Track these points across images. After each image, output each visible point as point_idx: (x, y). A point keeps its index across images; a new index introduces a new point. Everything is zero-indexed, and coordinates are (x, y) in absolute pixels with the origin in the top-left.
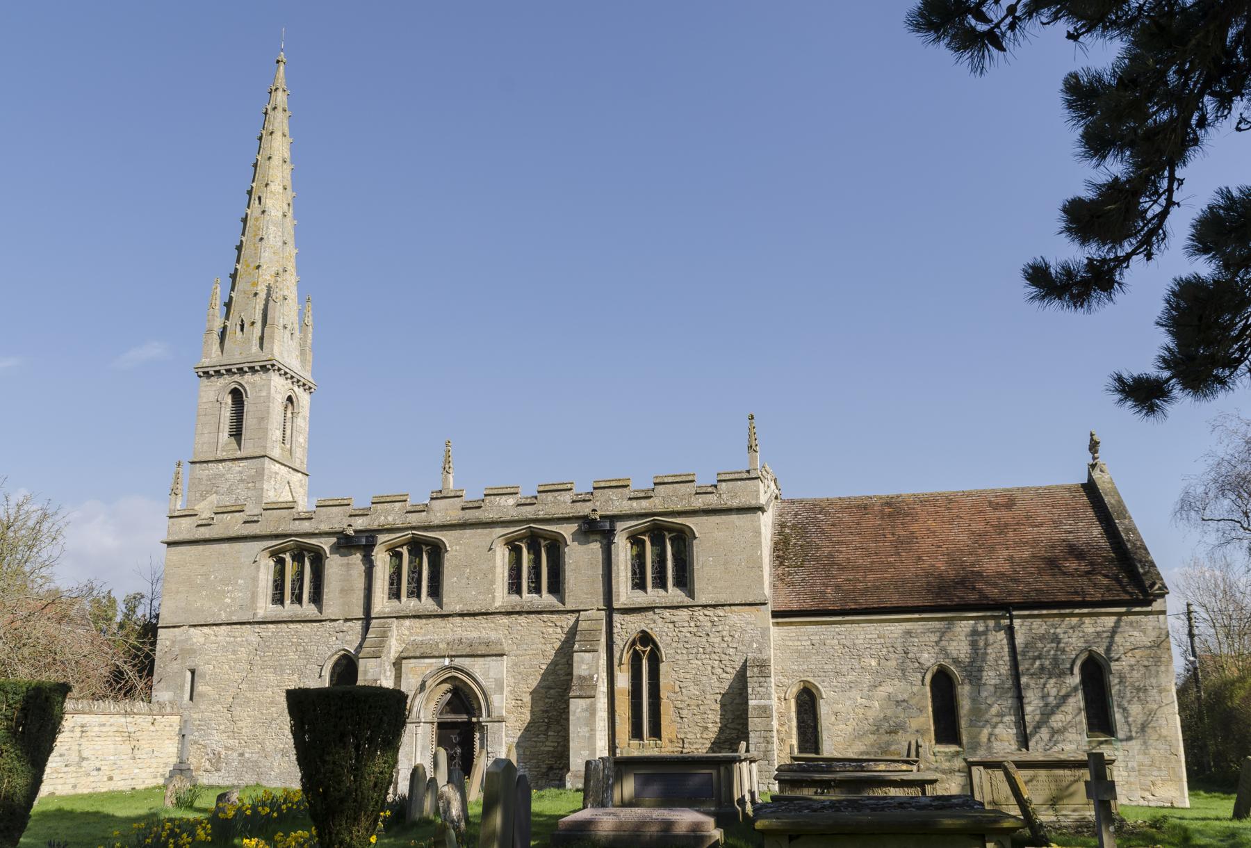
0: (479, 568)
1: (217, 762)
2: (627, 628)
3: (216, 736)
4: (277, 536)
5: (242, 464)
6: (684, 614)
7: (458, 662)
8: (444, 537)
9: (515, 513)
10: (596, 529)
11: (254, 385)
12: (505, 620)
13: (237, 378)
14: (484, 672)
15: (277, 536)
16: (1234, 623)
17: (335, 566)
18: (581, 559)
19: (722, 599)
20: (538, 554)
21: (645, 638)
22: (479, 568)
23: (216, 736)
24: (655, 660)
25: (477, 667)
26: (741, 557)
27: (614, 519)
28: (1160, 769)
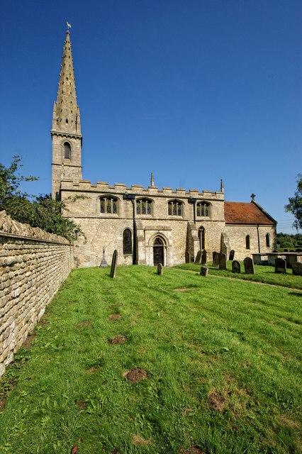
0: (160, 207)
1: (88, 259)
2: (198, 225)
3: (87, 251)
4: (103, 193)
5: (74, 168)
6: (210, 222)
7: (161, 232)
8: (154, 199)
9: (171, 195)
10: (192, 201)
11: (74, 143)
12: (169, 222)
13: (68, 139)
14: (167, 234)
15: (103, 193)
16: (21, 431)
17: (122, 203)
18: (187, 208)
19: (217, 219)
20: (175, 205)
21: (202, 227)
22: (160, 207)
23: (87, 251)
24: (203, 231)
25: (165, 233)
26: (218, 209)
27: (196, 199)
28: (152, 371)
